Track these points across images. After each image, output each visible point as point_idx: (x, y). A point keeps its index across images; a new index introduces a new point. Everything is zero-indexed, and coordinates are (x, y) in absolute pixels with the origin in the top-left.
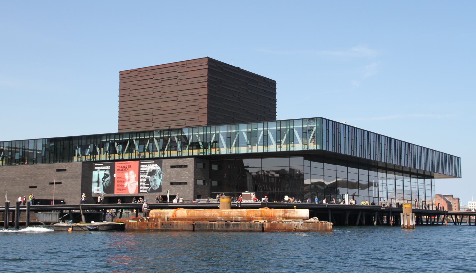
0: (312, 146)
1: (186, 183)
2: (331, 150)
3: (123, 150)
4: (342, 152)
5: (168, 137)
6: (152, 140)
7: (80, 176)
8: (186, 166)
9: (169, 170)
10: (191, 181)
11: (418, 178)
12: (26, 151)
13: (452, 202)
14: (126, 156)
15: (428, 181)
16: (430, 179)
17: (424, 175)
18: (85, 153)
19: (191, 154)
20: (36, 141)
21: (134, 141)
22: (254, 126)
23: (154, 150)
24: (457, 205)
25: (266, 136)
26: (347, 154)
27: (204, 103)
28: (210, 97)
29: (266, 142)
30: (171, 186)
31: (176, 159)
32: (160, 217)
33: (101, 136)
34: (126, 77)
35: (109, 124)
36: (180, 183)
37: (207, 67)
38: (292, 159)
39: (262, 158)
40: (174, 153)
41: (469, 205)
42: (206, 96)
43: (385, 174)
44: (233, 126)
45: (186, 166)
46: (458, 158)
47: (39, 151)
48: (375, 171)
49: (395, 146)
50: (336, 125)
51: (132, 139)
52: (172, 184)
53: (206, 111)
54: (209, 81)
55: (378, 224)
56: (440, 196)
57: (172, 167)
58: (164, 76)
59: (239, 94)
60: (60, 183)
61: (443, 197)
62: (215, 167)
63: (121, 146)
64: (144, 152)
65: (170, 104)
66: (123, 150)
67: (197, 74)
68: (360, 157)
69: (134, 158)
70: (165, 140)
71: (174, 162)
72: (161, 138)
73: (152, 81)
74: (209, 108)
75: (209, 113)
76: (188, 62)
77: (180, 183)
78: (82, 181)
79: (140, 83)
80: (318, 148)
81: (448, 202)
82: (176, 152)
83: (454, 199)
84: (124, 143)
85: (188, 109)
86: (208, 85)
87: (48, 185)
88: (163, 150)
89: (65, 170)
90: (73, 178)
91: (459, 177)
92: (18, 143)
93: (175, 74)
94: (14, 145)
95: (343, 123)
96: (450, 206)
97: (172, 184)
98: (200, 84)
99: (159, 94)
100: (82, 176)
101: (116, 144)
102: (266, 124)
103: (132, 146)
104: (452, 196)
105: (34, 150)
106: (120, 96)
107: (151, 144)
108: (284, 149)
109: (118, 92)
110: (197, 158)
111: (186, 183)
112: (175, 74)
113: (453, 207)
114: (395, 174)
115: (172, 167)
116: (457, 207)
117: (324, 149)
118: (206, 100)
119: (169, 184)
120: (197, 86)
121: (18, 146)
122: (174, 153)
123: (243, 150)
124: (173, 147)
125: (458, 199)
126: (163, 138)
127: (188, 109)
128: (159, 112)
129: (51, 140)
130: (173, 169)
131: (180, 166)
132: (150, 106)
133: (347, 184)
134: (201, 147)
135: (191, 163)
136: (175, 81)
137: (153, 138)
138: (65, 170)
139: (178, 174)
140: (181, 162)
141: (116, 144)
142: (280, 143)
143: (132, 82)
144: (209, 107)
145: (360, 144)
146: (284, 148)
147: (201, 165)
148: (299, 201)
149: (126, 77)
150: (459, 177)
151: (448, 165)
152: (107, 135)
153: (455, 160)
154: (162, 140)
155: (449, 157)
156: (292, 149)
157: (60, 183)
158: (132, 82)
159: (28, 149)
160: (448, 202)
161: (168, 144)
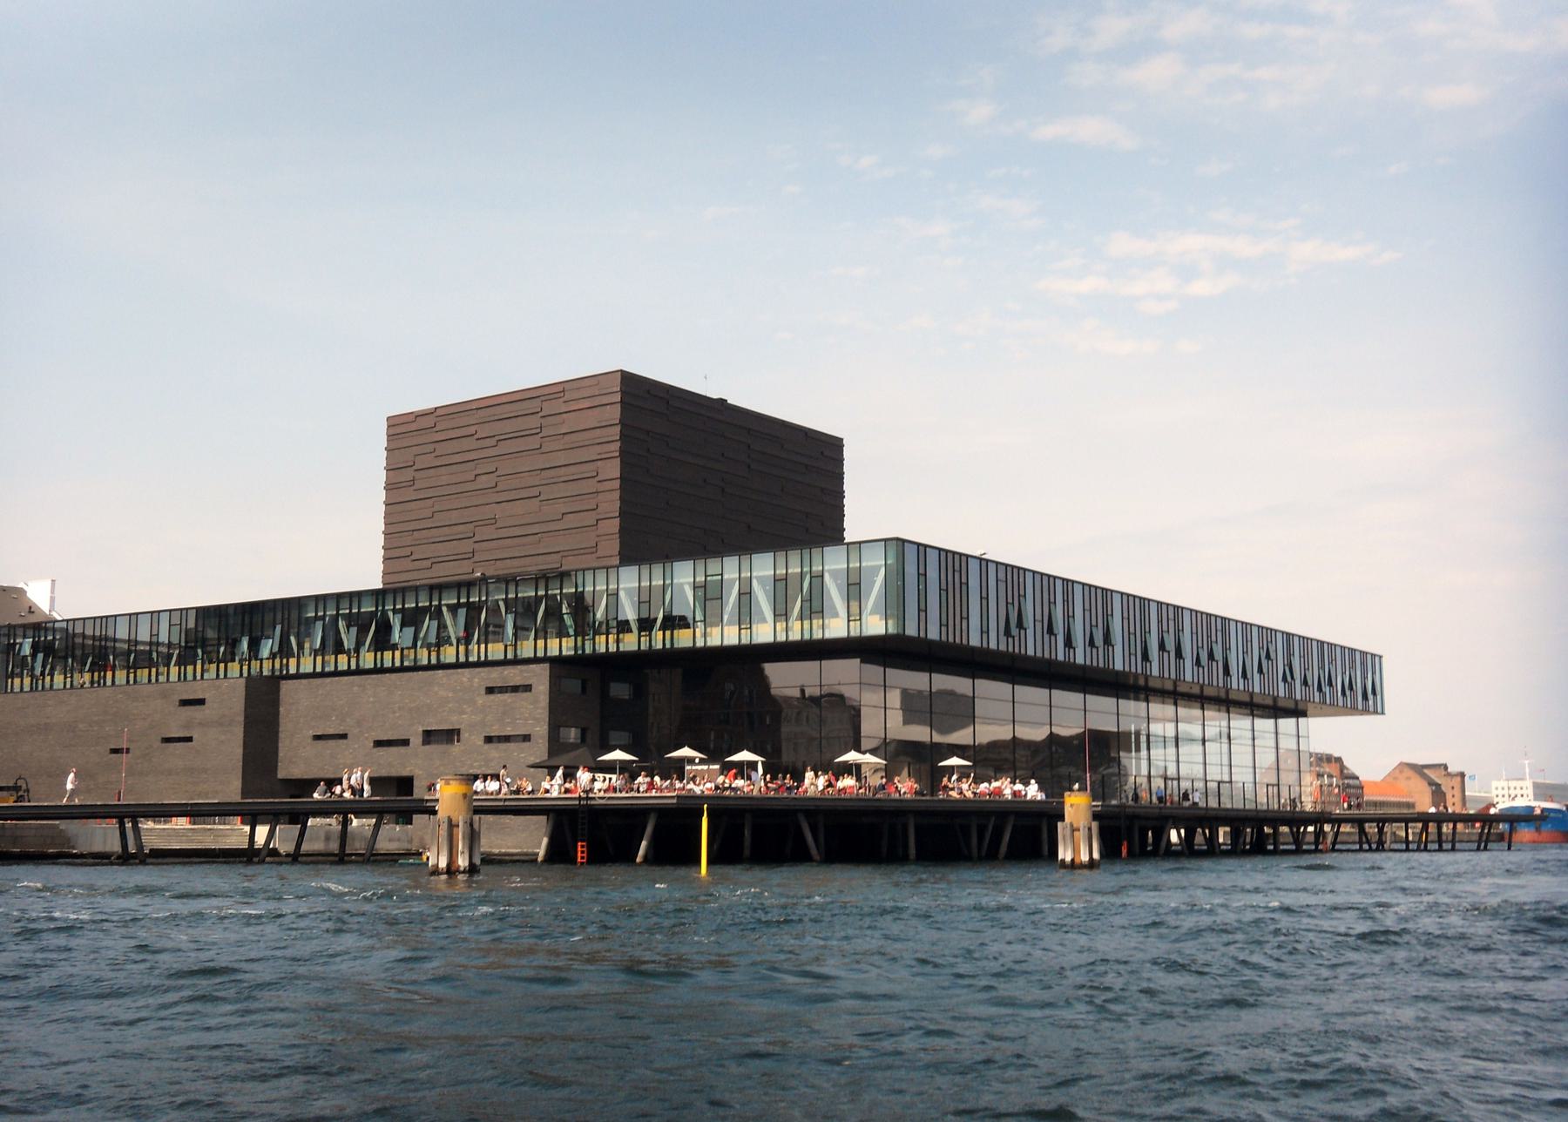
0: (875, 626)
1: (526, 738)
2: (933, 634)
3: (359, 644)
4: (975, 641)
5: (538, 600)
6: (438, 614)
7: (241, 718)
8: (528, 688)
9: (482, 699)
10: (541, 730)
11: (1276, 717)
12: (110, 644)
14: (368, 659)
15: (1287, 724)
16: (1293, 720)
17: (1276, 710)
18: (257, 651)
19: (540, 654)
20: (133, 617)
21: (390, 614)
22: (714, 566)
23: (442, 640)
24: (1457, 792)
25: (746, 595)
26: (993, 646)
27: (611, 503)
28: (628, 482)
29: (746, 613)
30: (487, 746)
31: (500, 669)
33: (298, 603)
34: (408, 434)
35: (361, 569)
36: (507, 739)
37: (618, 398)
38: (828, 664)
39: (821, 659)
40: (496, 651)
41: (1494, 793)
42: (617, 484)
43: (1144, 704)
44: (657, 569)
45: (528, 688)
46: (1373, 656)
47: (144, 643)
48: (1137, 699)
49: (1160, 621)
50: (953, 562)
51: (384, 612)
52: (489, 740)
53: (615, 525)
55: (1131, 854)
57: (490, 690)
58: (442, 550)
59: (730, 474)
60: (189, 739)
61: (1419, 769)
62: (620, 690)
63: (354, 630)
64: (415, 646)
65: (518, 508)
66: (359, 644)
67: (591, 419)
68: (1039, 654)
69: (425, 662)
70: (473, 609)
71: (495, 676)
72: (459, 605)
76: (567, 386)
77: (507, 739)
78: (245, 732)
80: (891, 630)
82: (501, 646)
83: (1449, 775)
84: (412, 619)
85: (571, 521)
86: (622, 451)
87: (158, 744)
88: (467, 640)
90: (221, 725)
91: (1375, 712)
92: (89, 624)
93: (533, 422)
94: (79, 630)
95: (977, 554)
96: (1438, 794)
97: (489, 740)
98: (598, 449)
100: (246, 717)
101: (342, 624)
102: (745, 559)
103: (385, 628)
104: (1446, 767)
105: (151, 644)
106: (389, 487)
107: (435, 623)
108: (795, 636)
109: (382, 476)
110: (558, 663)
111: (526, 738)
112: (533, 422)
113: (1449, 797)
114: (1176, 704)
115: (490, 690)
116: (1457, 799)
117: (911, 631)
119: (480, 742)
120: (592, 453)
121: (89, 632)
122: (496, 651)
123: (764, 633)
124: (492, 632)
125: (1462, 775)
126: (468, 605)
127: (571, 521)
128: (488, 533)
129: (204, 613)
130: (492, 697)
131: (515, 689)
133: (1040, 737)
134: (571, 632)
135: (540, 678)
136: (533, 442)
137: (440, 606)
138: (201, 702)
139: (504, 713)
140: (514, 675)
141: (342, 624)
142: (786, 616)
143: (425, 450)
145: (1038, 617)
146: (796, 632)
147: (573, 685)
149: (408, 434)
150: (1378, 711)
151: (1348, 681)
152: (339, 597)
153: (1368, 662)
154: (462, 612)
155: (1343, 655)
156: (818, 635)
157: (189, 739)
158: (425, 450)
159: (115, 640)
160: (1431, 783)
161: (480, 623)
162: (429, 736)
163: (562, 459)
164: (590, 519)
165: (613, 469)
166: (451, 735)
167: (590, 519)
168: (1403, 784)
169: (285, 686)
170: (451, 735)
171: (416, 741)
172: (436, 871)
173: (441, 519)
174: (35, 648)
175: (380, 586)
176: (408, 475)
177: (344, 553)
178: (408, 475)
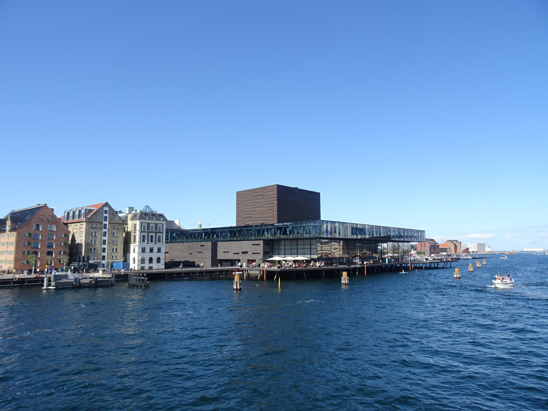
9: (252, 246)
10: (262, 252)
13: (457, 244)
28: (278, 205)
32: (144, 289)
35: (231, 221)
54: (278, 197)
56: (450, 241)
58: (257, 194)
61: (451, 241)
73: (251, 197)
74: (278, 211)
75: (278, 214)
79: (246, 197)
81: (455, 244)
89: (134, 258)
93: (250, 215)
99: (254, 204)
106: (237, 204)
109: (236, 203)
118: (12, 248)
132: (250, 210)
136: (262, 197)
138: (134, 258)
140: (257, 242)
143: (244, 198)
144: (278, 211)
148: (365, 251)
160: (455, 244)
162: (243, 253)
163: (266, 200)
164: (272, 211)
165: (276, 202)
166: (246, 252)
167: (272, 211)
168: (448, 244)
169: (219, 243)
170: (246, 252)
171: (241, 253)
172: (234, 289)
173: (246, 210)
174: (176, 235)
175: (234, 225)
176: (240, 202)
177: (228, 219)
178: (240, 202)
